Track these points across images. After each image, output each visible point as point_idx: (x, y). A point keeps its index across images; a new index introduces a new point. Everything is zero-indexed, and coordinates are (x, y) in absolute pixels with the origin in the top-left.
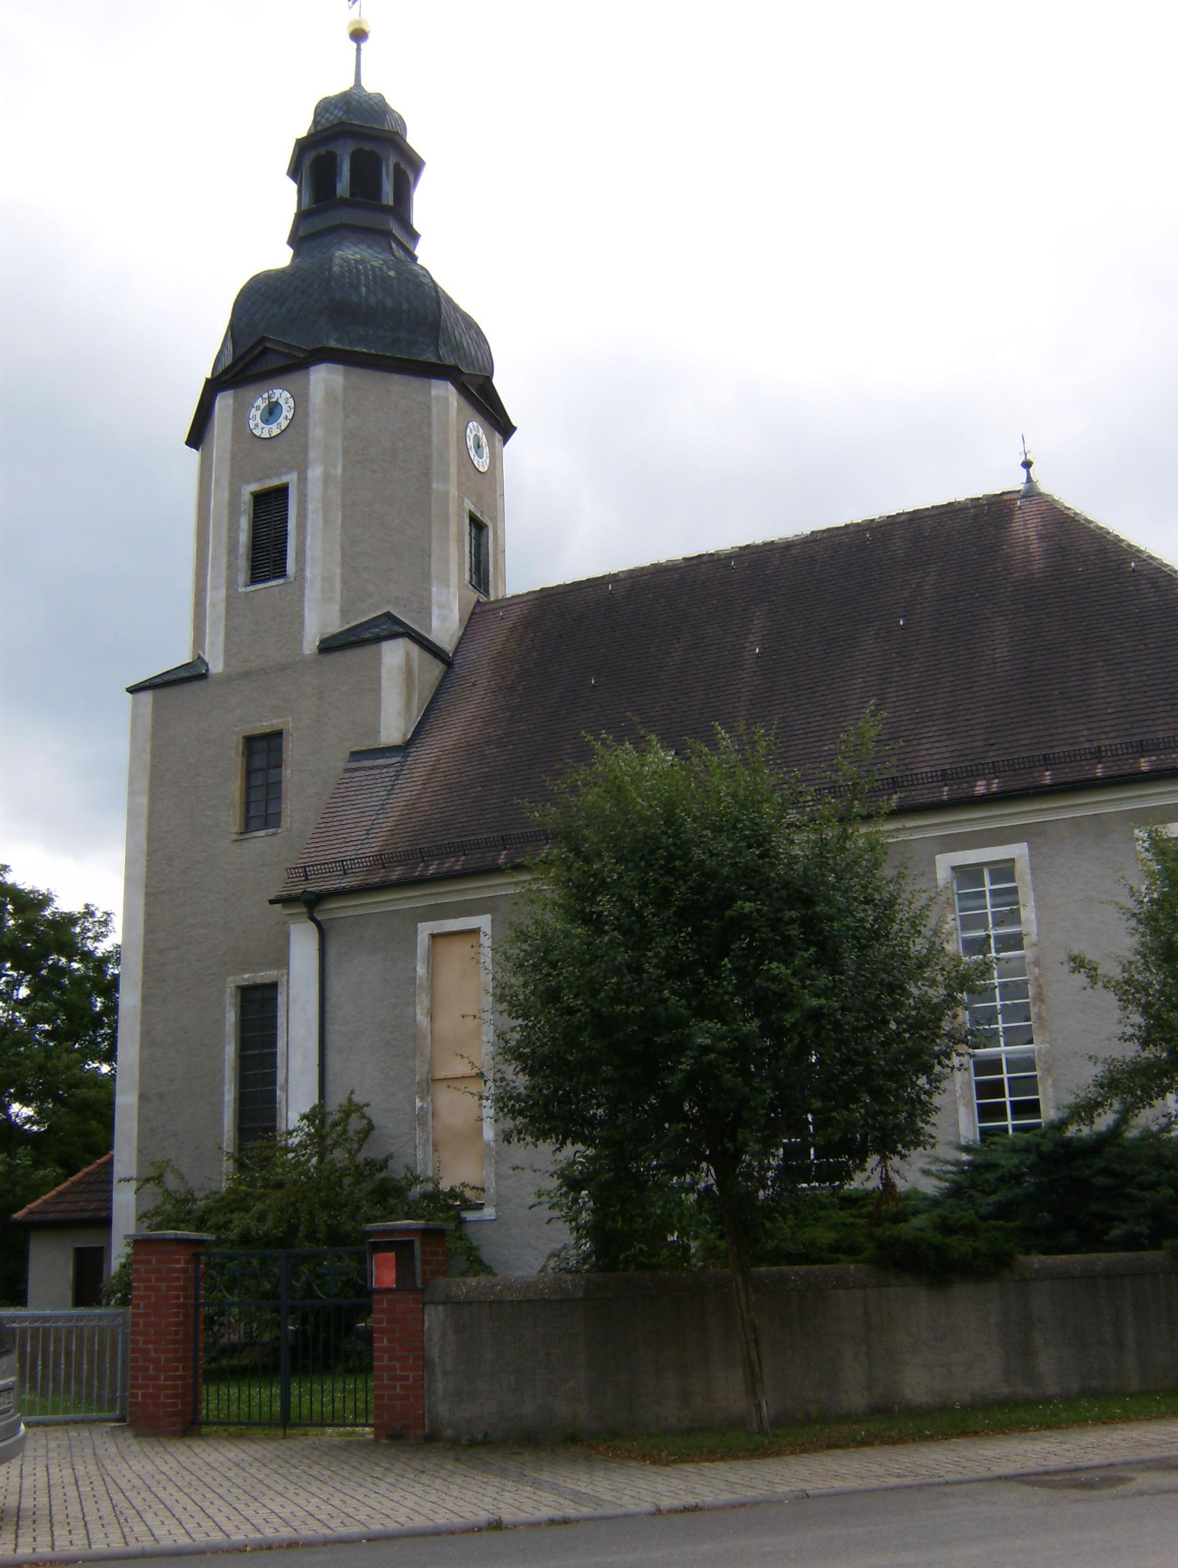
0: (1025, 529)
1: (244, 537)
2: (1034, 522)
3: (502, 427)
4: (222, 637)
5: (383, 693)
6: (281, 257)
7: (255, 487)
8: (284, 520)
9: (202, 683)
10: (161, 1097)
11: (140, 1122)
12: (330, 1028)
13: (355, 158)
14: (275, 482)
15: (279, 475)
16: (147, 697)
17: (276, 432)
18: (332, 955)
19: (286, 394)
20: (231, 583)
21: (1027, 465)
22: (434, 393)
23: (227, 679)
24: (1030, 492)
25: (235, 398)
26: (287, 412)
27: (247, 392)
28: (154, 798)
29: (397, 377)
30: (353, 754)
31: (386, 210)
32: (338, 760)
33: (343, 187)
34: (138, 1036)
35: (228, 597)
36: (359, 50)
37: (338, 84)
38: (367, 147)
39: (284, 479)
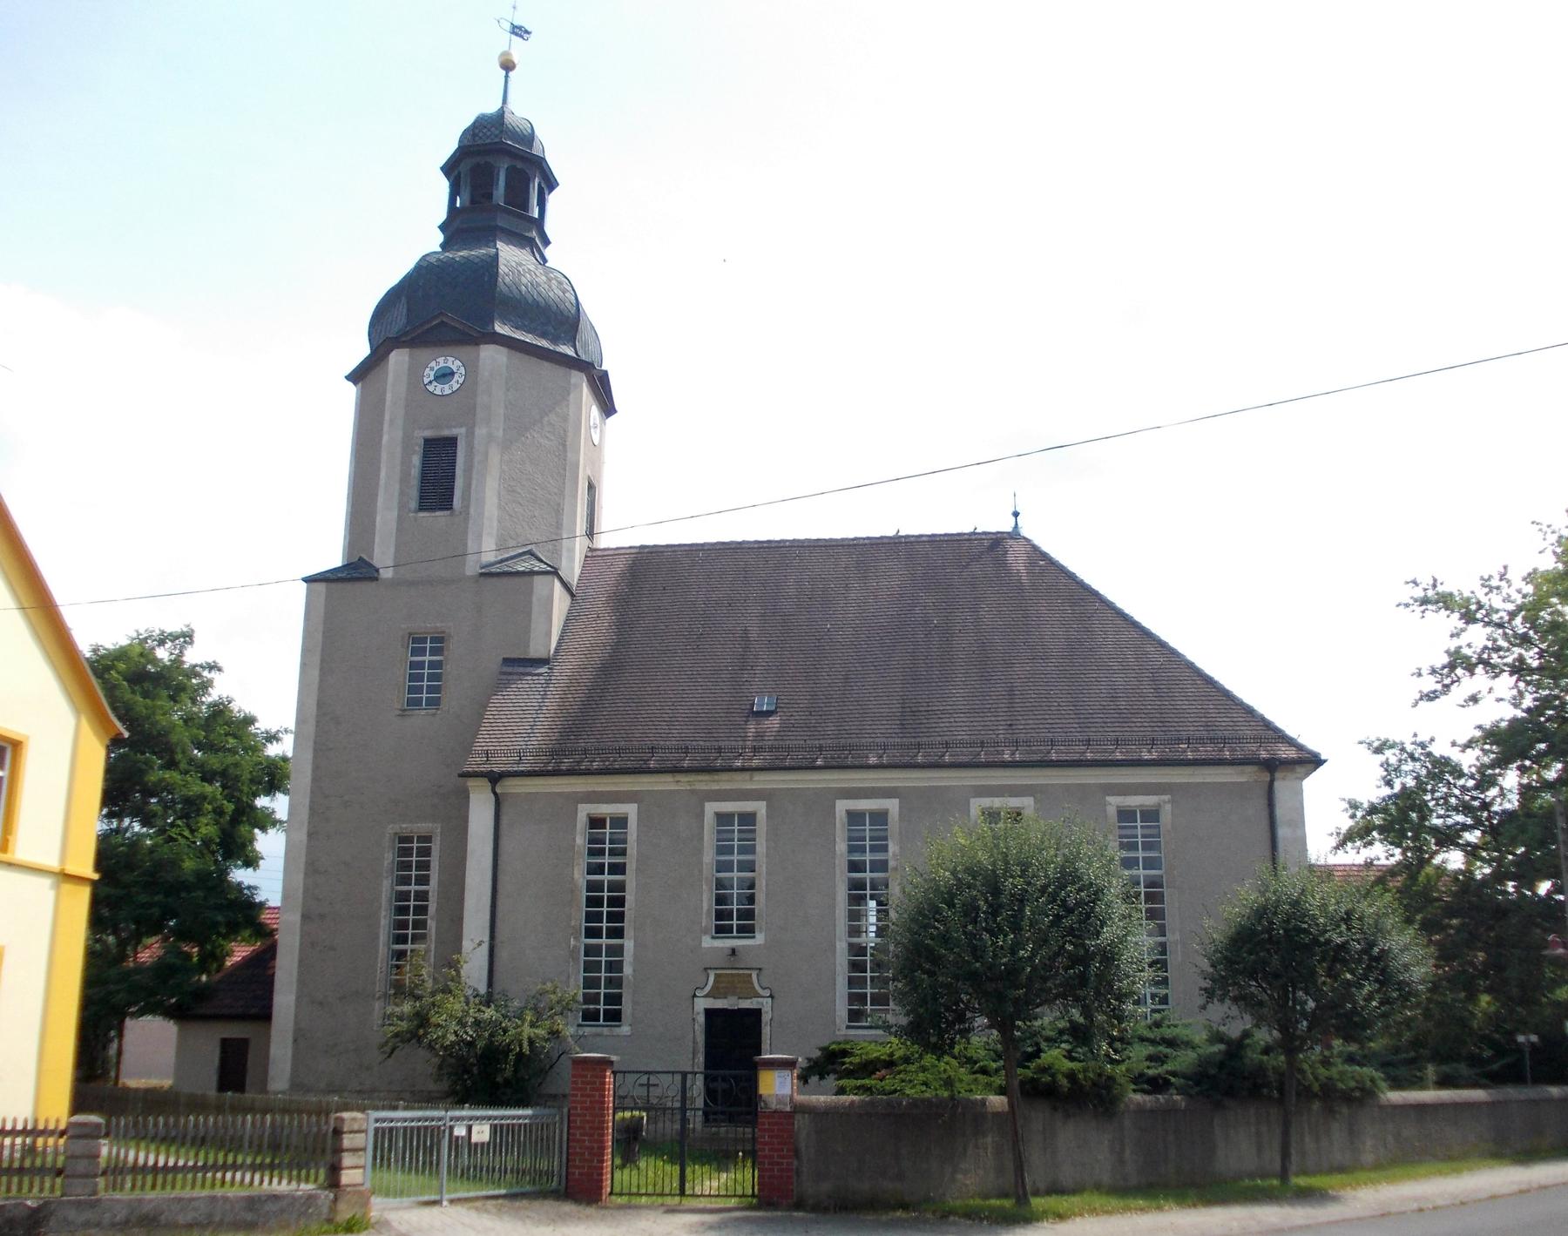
0: (1017, 559)
1: (415, 472)
2: (1022, 558)
3: (608, 409)
4: (392, 549)
5: (534, 616)
6: (432, 241)
7: (429, 434)
8: (453, 464)
9: (374, 584)
10: (322, 916)
11: (302, 937)
12: (501, 877)
13: (511, 172)
14: (446, 433)
15: (450, 427)
16: (321, 587)
17: (447, 392)
18: (504, 820)
19: (458, 363)
20: (402, 506)
21: (1016, 514)
22: (573, 381)
23: (394, 583)
24: (1015, 535)
25: (411, 356)
26: (458, 379)
27: (423, 353)
28: (325, 670)
29: (546, 364)
30: (505, 660)
31: (532, 219)
32: (493, 664)
33: (499, 193)
34: (302, 866)
35: (399, 517)
36: (507, 77)
37: (492, 108)
38: (519, 165)
39: (454, 432)
